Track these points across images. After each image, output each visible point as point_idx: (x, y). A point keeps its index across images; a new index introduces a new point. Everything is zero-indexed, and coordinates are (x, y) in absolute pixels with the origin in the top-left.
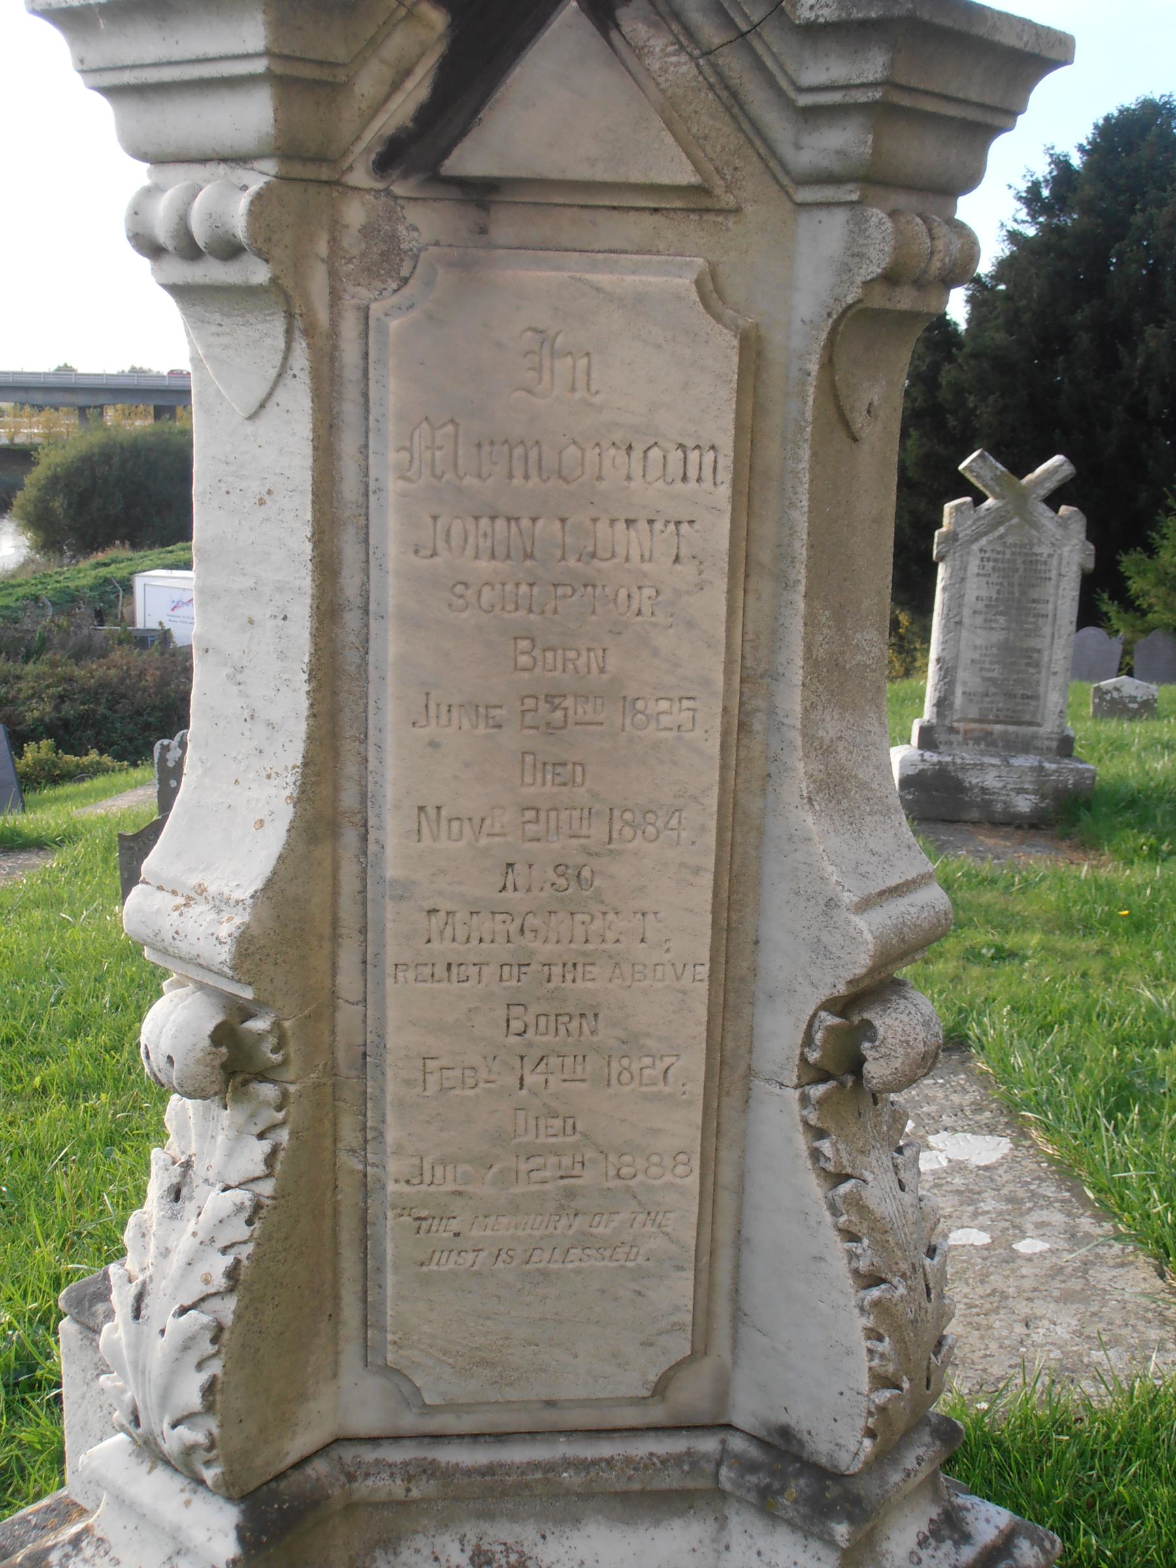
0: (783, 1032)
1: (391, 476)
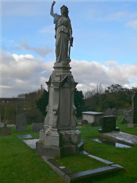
0: (72, 113)
1: (61, 95)
